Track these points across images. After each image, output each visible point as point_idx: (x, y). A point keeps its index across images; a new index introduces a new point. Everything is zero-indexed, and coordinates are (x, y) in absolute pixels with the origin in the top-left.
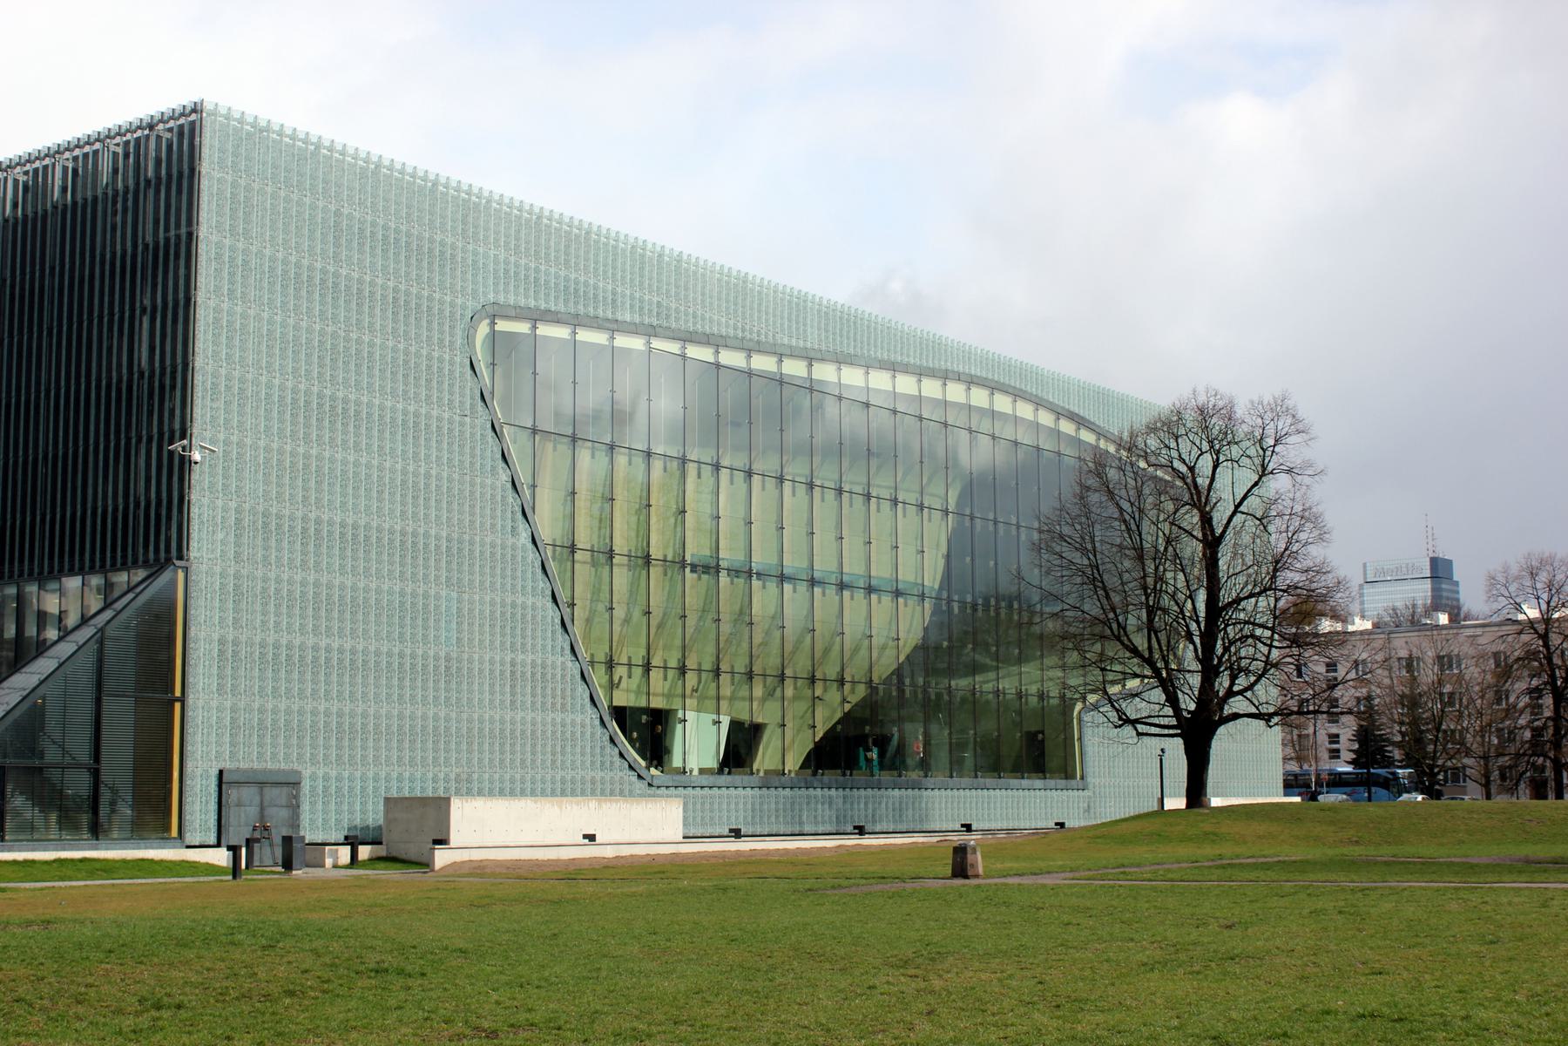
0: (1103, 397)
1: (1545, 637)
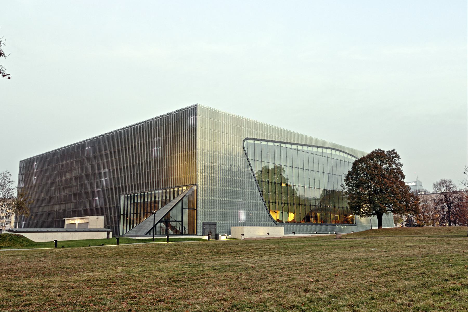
0: (357, 151)
1: (446, 196)
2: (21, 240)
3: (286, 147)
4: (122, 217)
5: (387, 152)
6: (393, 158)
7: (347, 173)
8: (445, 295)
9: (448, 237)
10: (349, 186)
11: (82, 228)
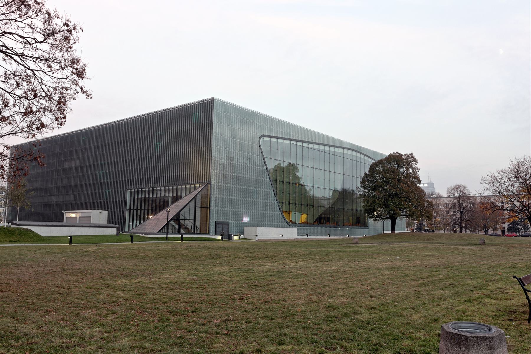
1: (459, 201)
2: (30, 235)
5: (405, 155)
6: (411, 162)
7: (363, 175)
8: (473, 302)
9: (461, 245)
11: (84, 222)
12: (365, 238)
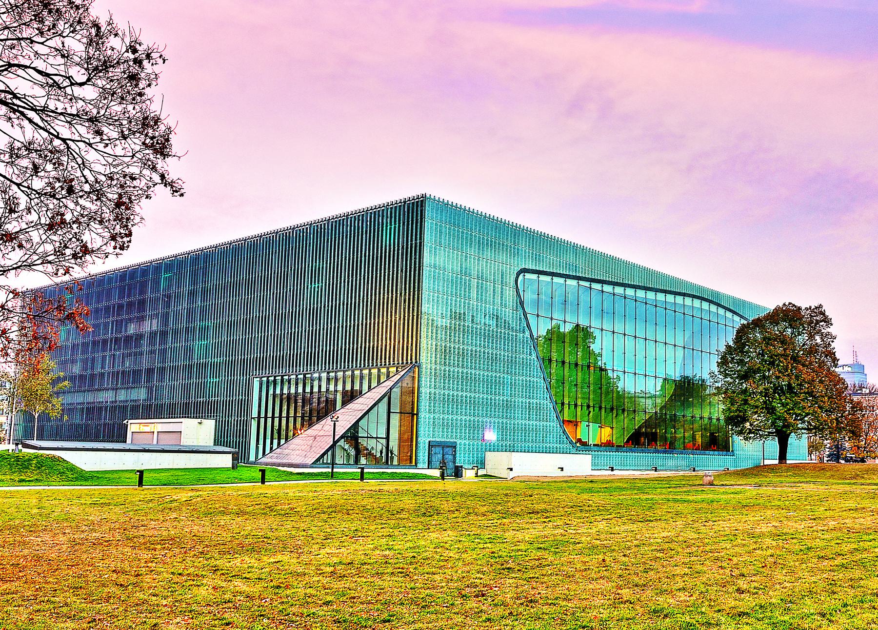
3: (603, 291)
4: (254, 424)
5: (807, 309)
6: (818, 322)
7: (723, 349)
10: (726, 376)
11: (167, 442)
12: (727, 473)
